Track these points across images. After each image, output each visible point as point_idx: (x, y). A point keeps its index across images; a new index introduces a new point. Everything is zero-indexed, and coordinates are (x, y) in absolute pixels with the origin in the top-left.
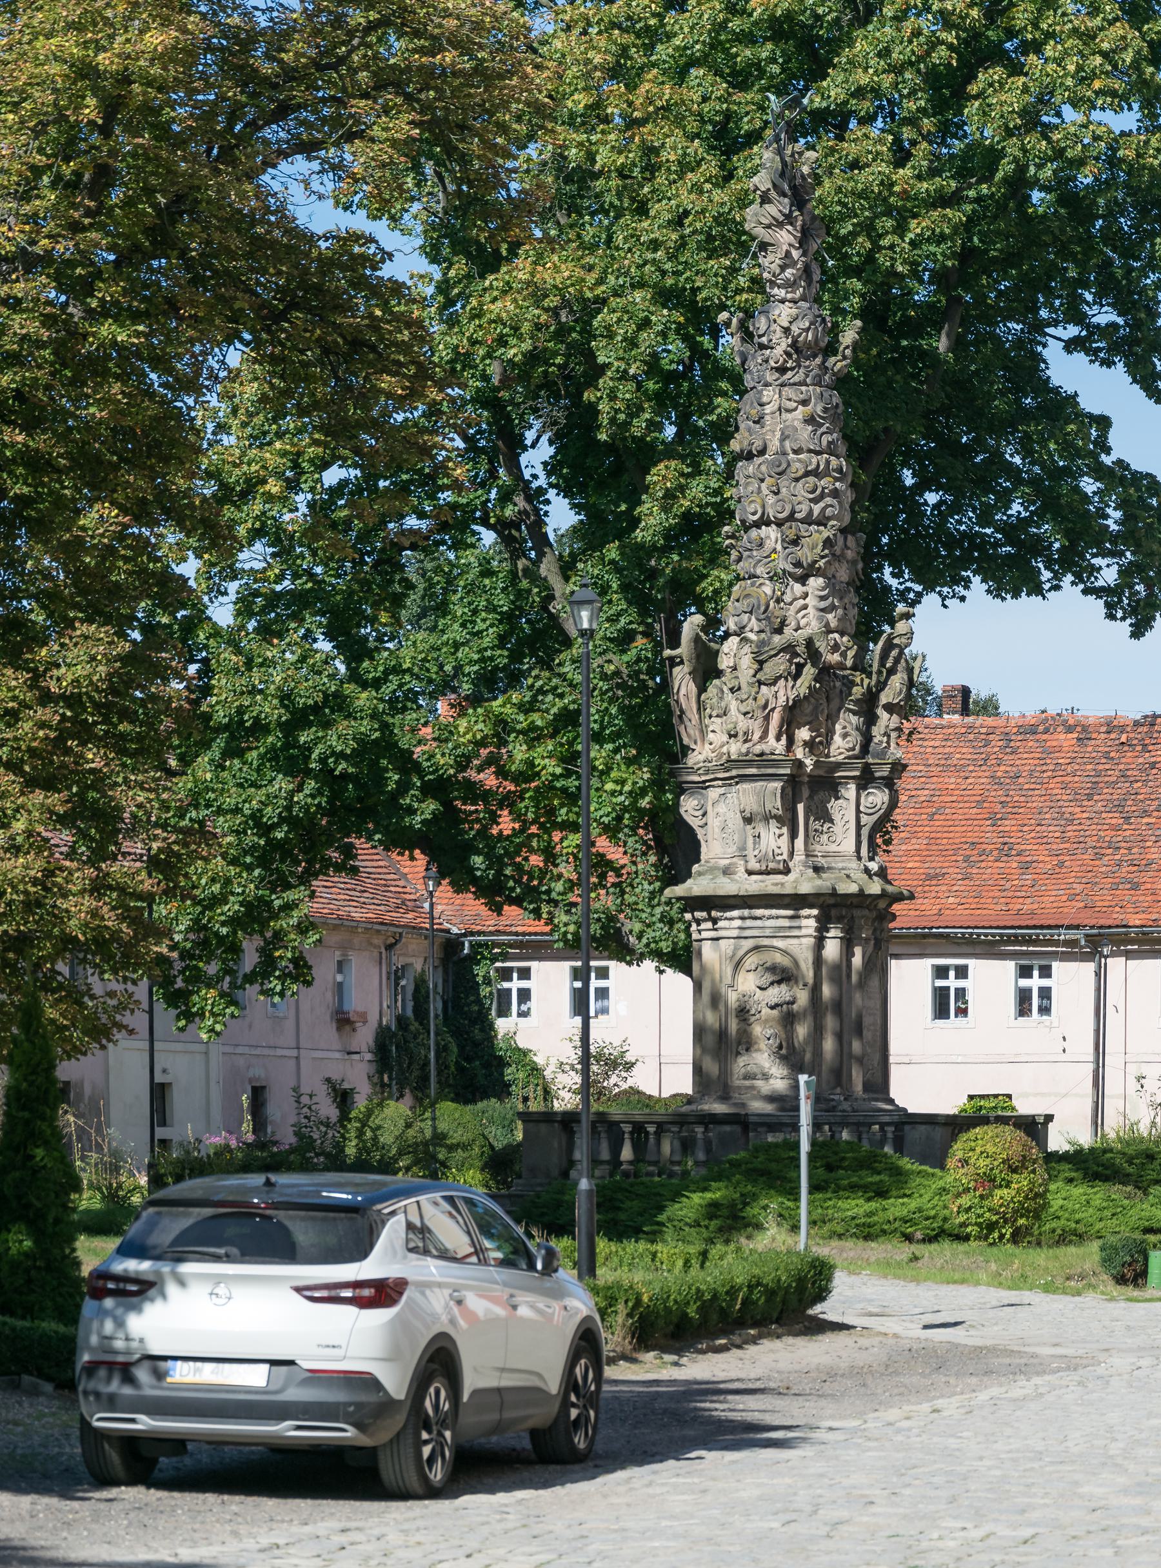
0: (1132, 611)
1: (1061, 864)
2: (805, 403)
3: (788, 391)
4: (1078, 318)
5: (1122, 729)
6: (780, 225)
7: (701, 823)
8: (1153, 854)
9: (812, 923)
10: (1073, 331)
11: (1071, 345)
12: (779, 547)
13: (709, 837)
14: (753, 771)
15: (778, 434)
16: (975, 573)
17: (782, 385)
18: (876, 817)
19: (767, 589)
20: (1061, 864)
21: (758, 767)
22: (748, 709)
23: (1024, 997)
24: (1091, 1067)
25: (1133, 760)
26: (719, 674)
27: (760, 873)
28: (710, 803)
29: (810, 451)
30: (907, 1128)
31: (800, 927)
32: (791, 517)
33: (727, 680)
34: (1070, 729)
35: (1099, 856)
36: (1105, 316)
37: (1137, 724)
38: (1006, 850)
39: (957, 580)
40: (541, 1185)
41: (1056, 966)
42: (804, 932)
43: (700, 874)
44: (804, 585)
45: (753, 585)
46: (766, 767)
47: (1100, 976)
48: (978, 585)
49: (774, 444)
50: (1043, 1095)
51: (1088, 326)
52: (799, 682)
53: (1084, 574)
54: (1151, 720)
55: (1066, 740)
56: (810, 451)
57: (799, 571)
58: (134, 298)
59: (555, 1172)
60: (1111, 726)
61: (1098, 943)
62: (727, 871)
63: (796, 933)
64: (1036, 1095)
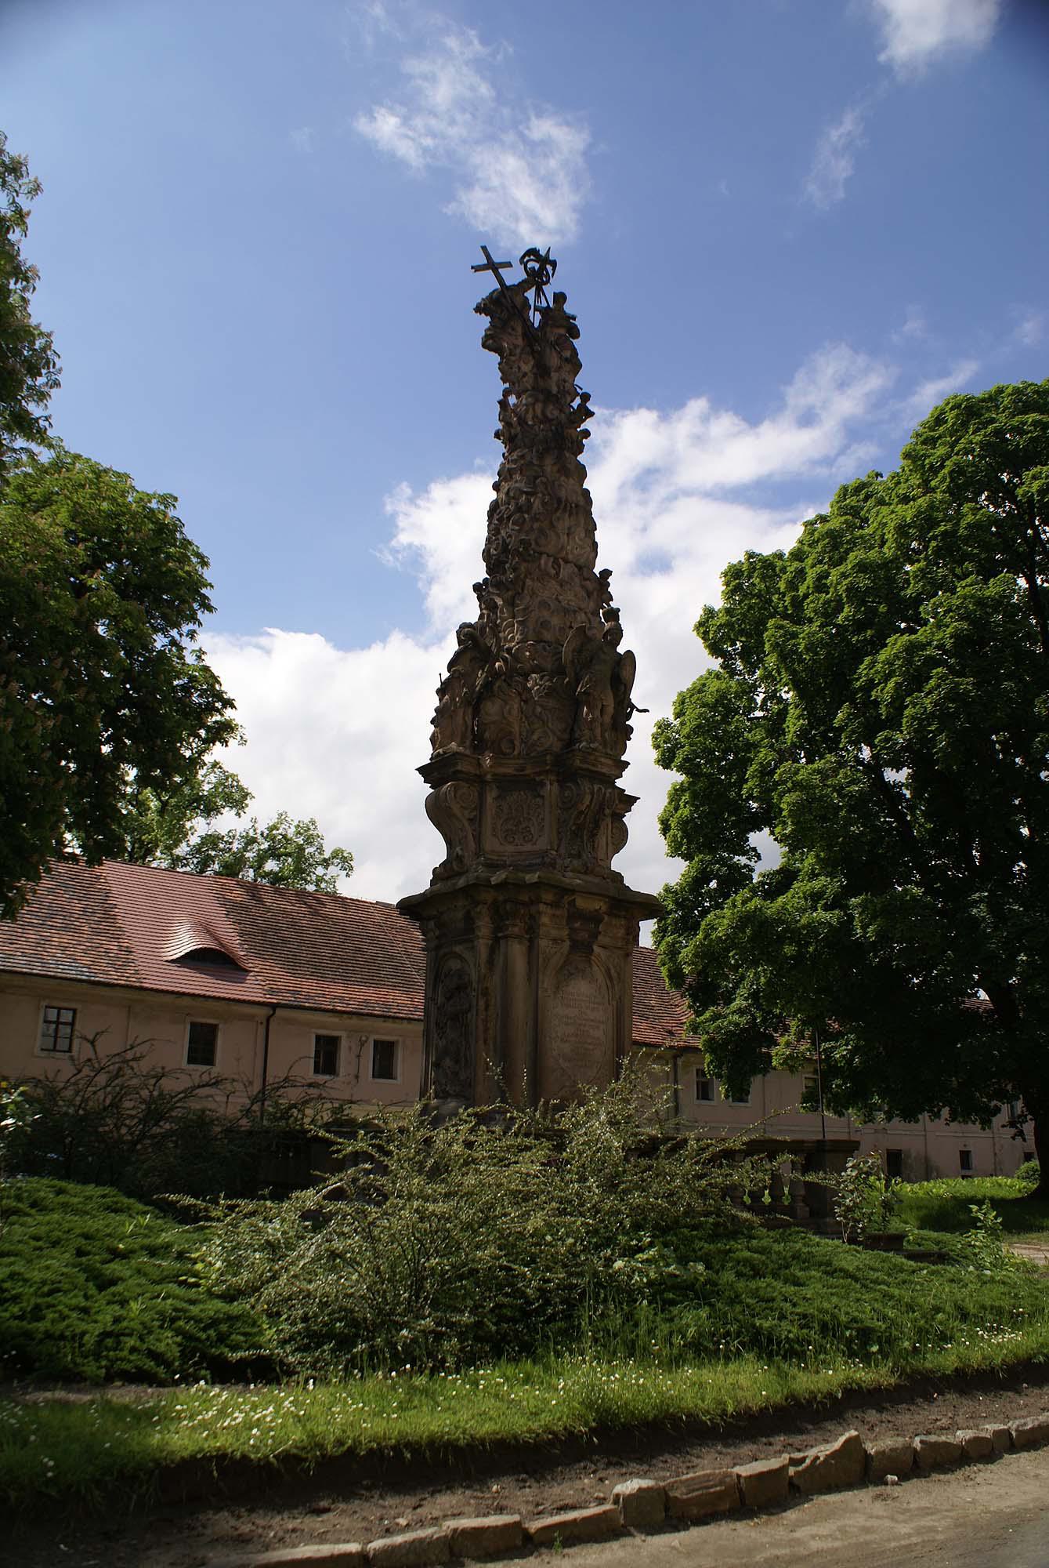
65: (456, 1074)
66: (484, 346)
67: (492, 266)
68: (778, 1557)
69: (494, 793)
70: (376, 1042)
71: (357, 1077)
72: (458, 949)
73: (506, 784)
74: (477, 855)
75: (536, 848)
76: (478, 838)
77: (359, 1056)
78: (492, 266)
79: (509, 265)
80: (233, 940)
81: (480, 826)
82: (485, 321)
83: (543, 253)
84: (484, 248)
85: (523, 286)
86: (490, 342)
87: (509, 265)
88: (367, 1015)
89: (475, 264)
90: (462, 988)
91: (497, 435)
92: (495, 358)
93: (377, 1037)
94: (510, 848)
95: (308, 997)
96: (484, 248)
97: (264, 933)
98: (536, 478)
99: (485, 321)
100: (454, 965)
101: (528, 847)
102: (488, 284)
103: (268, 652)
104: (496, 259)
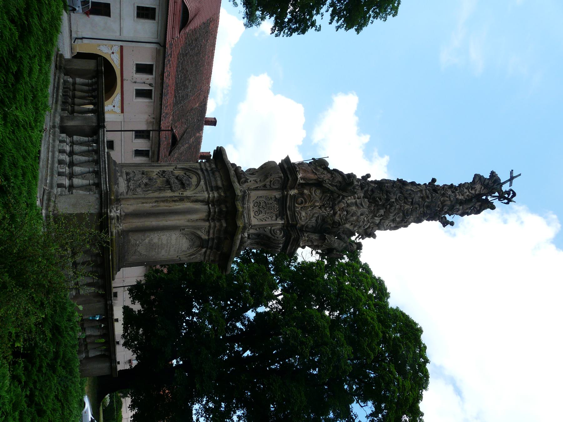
18: (270, 235)
65: (140, 186)
66: (476, 175)
67: (512, 178)
68: (46, 97)
69: (278, 196)
70: (151, 90)
71: (135, 82)
72: (202, 182)
73: (282, 201)
74: (249, 189)
75: (252, 218)
76: (256, 189)
77: (144, 83)
78: (512, 178)
79: (511, 185)
80: (191, 26)
81: (261, 190)
82: (487, 176)
83: (514, 199)
84: (520, 175)
85: (500, 191)
86: (478, 178)
87: (511, 185)
88: (163, 87)
89: (514, 171)
90: (183, 186)
91: (434, 180)
92: (470, 180)
93: (153, 91)
94: (252, 205)
95: (169, 61)
96: (520, 175)
97: (196, 40)
98: (419, 205)
99: (487, 176)
100: (194, 180)
101: (252, 214)
102: (503, 177)
103: (505, 222)
104: (514, 181)
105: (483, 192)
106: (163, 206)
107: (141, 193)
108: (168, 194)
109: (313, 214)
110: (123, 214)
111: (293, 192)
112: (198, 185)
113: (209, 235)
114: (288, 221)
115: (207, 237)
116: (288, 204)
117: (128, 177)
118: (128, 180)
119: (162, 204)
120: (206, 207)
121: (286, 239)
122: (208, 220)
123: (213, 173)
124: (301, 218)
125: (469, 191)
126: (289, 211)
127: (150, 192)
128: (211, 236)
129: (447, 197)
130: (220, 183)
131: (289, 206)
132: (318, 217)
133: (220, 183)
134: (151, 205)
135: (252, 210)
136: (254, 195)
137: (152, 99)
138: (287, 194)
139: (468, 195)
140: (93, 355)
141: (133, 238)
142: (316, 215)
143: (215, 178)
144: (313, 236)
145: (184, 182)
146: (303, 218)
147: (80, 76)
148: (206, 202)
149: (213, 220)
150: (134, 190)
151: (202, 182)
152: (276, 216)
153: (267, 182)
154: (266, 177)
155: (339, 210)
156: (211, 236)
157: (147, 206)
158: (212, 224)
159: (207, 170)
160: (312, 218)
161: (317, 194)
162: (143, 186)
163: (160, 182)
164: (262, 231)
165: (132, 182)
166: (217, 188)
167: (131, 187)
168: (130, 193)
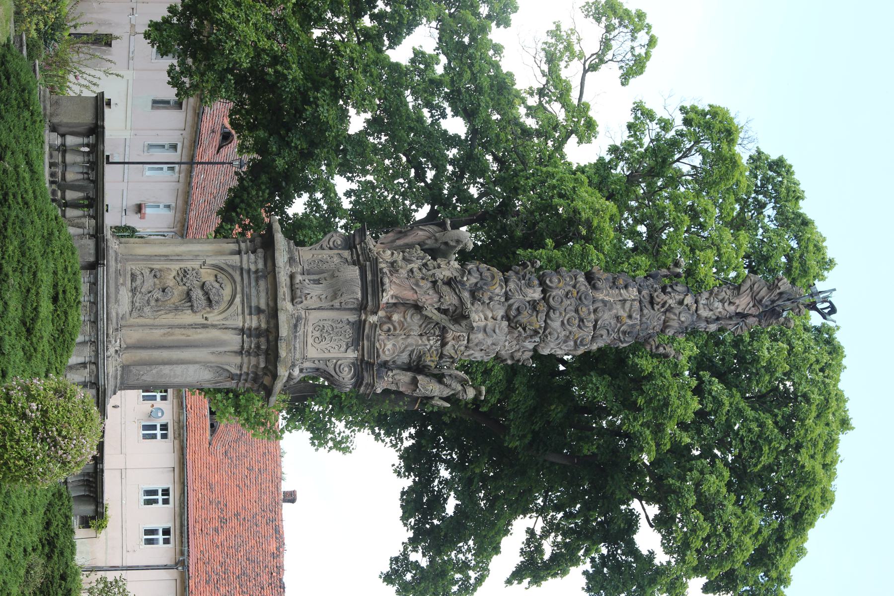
0: (395, 572)
1: (217, 547)
2: (630, 317)
3: (636, 304)
4: (545, 534)
5: (278, 573)
6: (753, 298)
7: (324, 246)
8: (223, 590)
9: (254, 324)
10: (538, 531)
11: (531, 532)
12: (528, 299)
13: (313, 252)
14: (369, 278)
15: (606, 298)
16: (414, 481)
17: (640, 302)
18: (333, 373)
19: (498, 291)
20: (217, 547)
21: (372, 281)
22: (415, 273)
23: (153, 532)
24: (119, 564)
25: (265, 579)
26: (434, 259)
27: (292, 285)
28: (340, 252)
29: (596, 321)
30: (94, 391)
31: (250, 314)
32: (550, 308)
33: (431, 263)
34: (278, 549)
35: (221, 564)
36: (547, 549)
37: (281, 580)
38: (223, 521)
39: (409, 469)
40: (45, 108)
41: (286, 487)
42: (248, 317)
43: (289, 244)
44: (503, 317)
45: (500, 280)
46: (373, 286)
47: (165, 567)
48: (407, 482)
49: (600, 296)
50: (106, 542)
51: (541, 537)
52: (436, 312)
53: (414, 542)
54: (282, 587)
55: (273, 547)
56: (596, 321)
57: (513, 313)
58: (395, 194)
59: (55, 120)
60: (280, 569)
61: (181, 564)
62: (291, 260)
63: (247, 311)
64: (106, 539)
73: (359, 327)
94: (310, 329)
101: (310, 340)
105: (750, 312)
106: (179, 336)
107: (149, 314)
108: (188, 317)
109: (406, 347)
110: (124, 346)
111: (373, 319)
112: (231, 302)
113: (241, 370)
114: (363, 355)
115: (238, 372)
116: (366, 331)
117: (134, 285)
118: (134, 291)
119: (177, 331)
120: (238, 338)
121: (357, 381)
122: (240, 353)
123: (257, 281)
124: (384, 352)
125: (723, 306)
126: (368, 340)
127: (163, 312)
128: (245, 369)
129: (675, 314)
130: (263, 306)
131: (368, 335)
132: (412, 351)
133: (263, 306)
134: (162, 331)
135: (310, 334)
136: (314, 316)
137: (176, 151)
138: (365, 321)
139: (720, 312)
140: (75, 362)
141: (134, 370)
142: (410, 349)
143: (258, 292)
144: (402, 377)
145: (212, 297)
146: (387, 353)
147: (73, 134)
148: (242, 331)
149: (249, 353)
150: (141, 309)
151: (238, 299)
152: (347, 345)
153: (336, 304)
154: (417, 122)
155: (453, 339)
156: (245, 369)
157: (157, 335)
158: (246, 359)
159: (249, 271)
160: (403, 352)
161: (414, 321)
162: (153, 303)
163: (177, 292)
164: (322, 365)
165: (139, 295)
166: (259, 311)
167: (137, 304)
168: (135, 314)
